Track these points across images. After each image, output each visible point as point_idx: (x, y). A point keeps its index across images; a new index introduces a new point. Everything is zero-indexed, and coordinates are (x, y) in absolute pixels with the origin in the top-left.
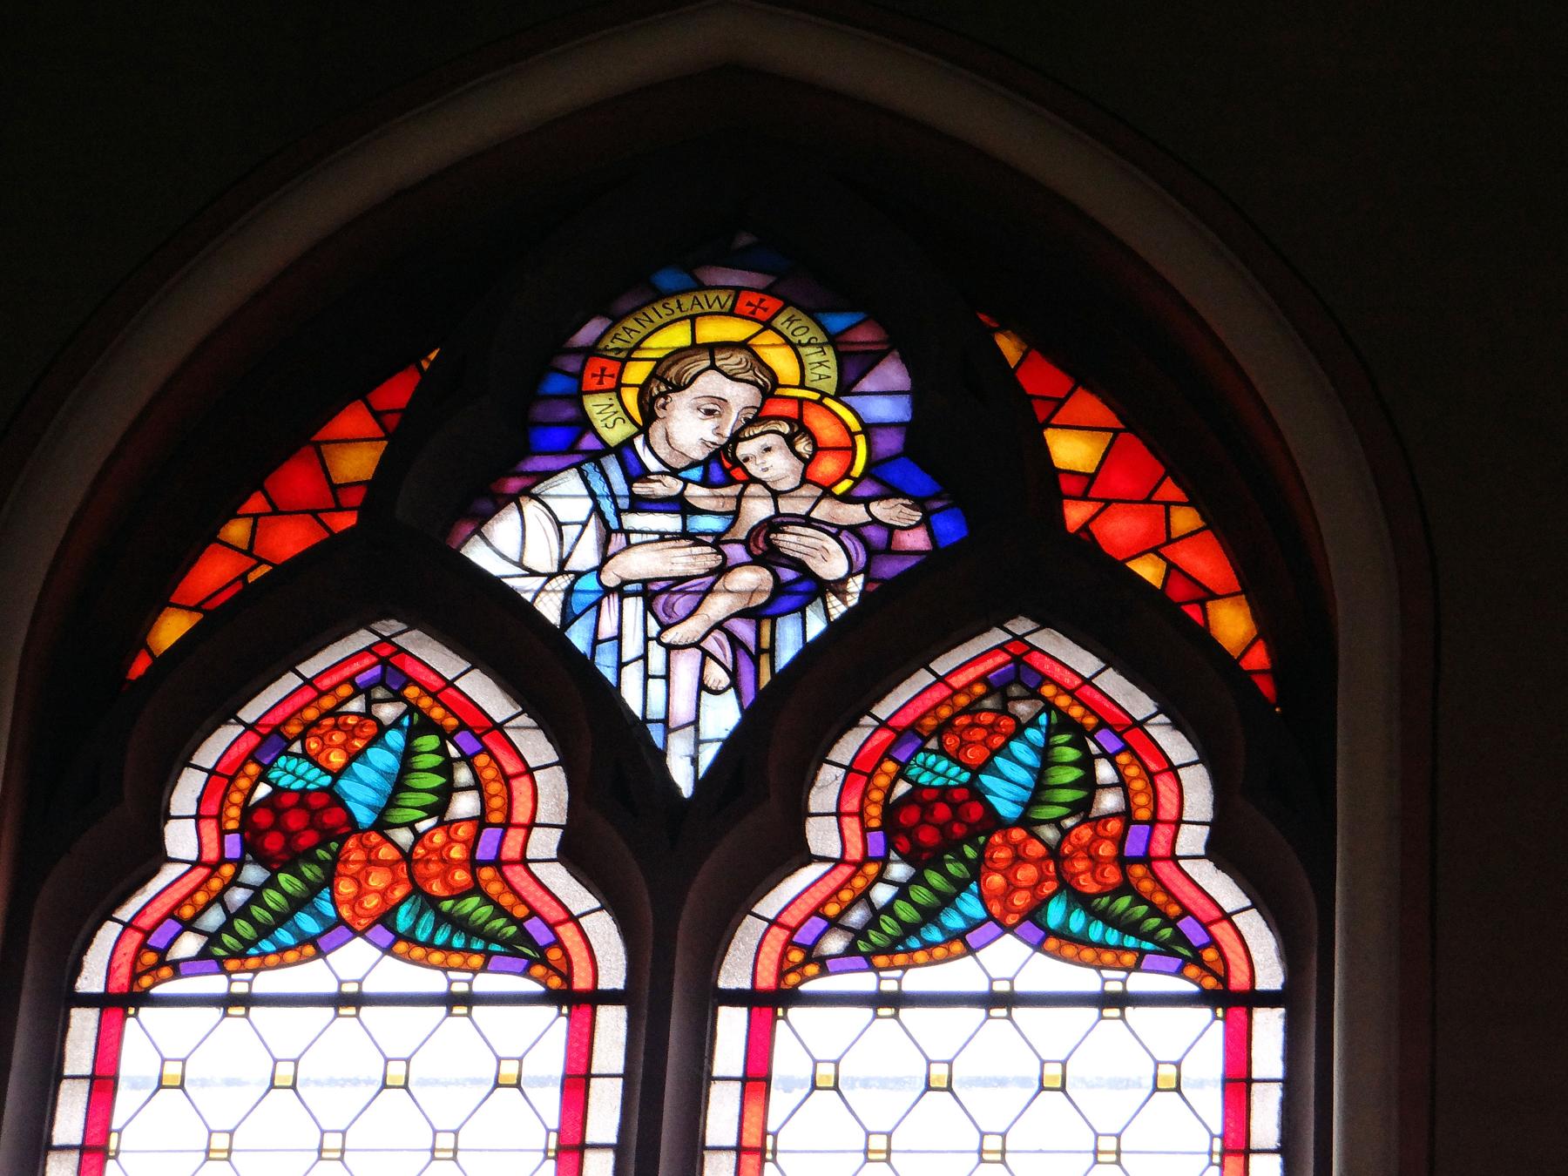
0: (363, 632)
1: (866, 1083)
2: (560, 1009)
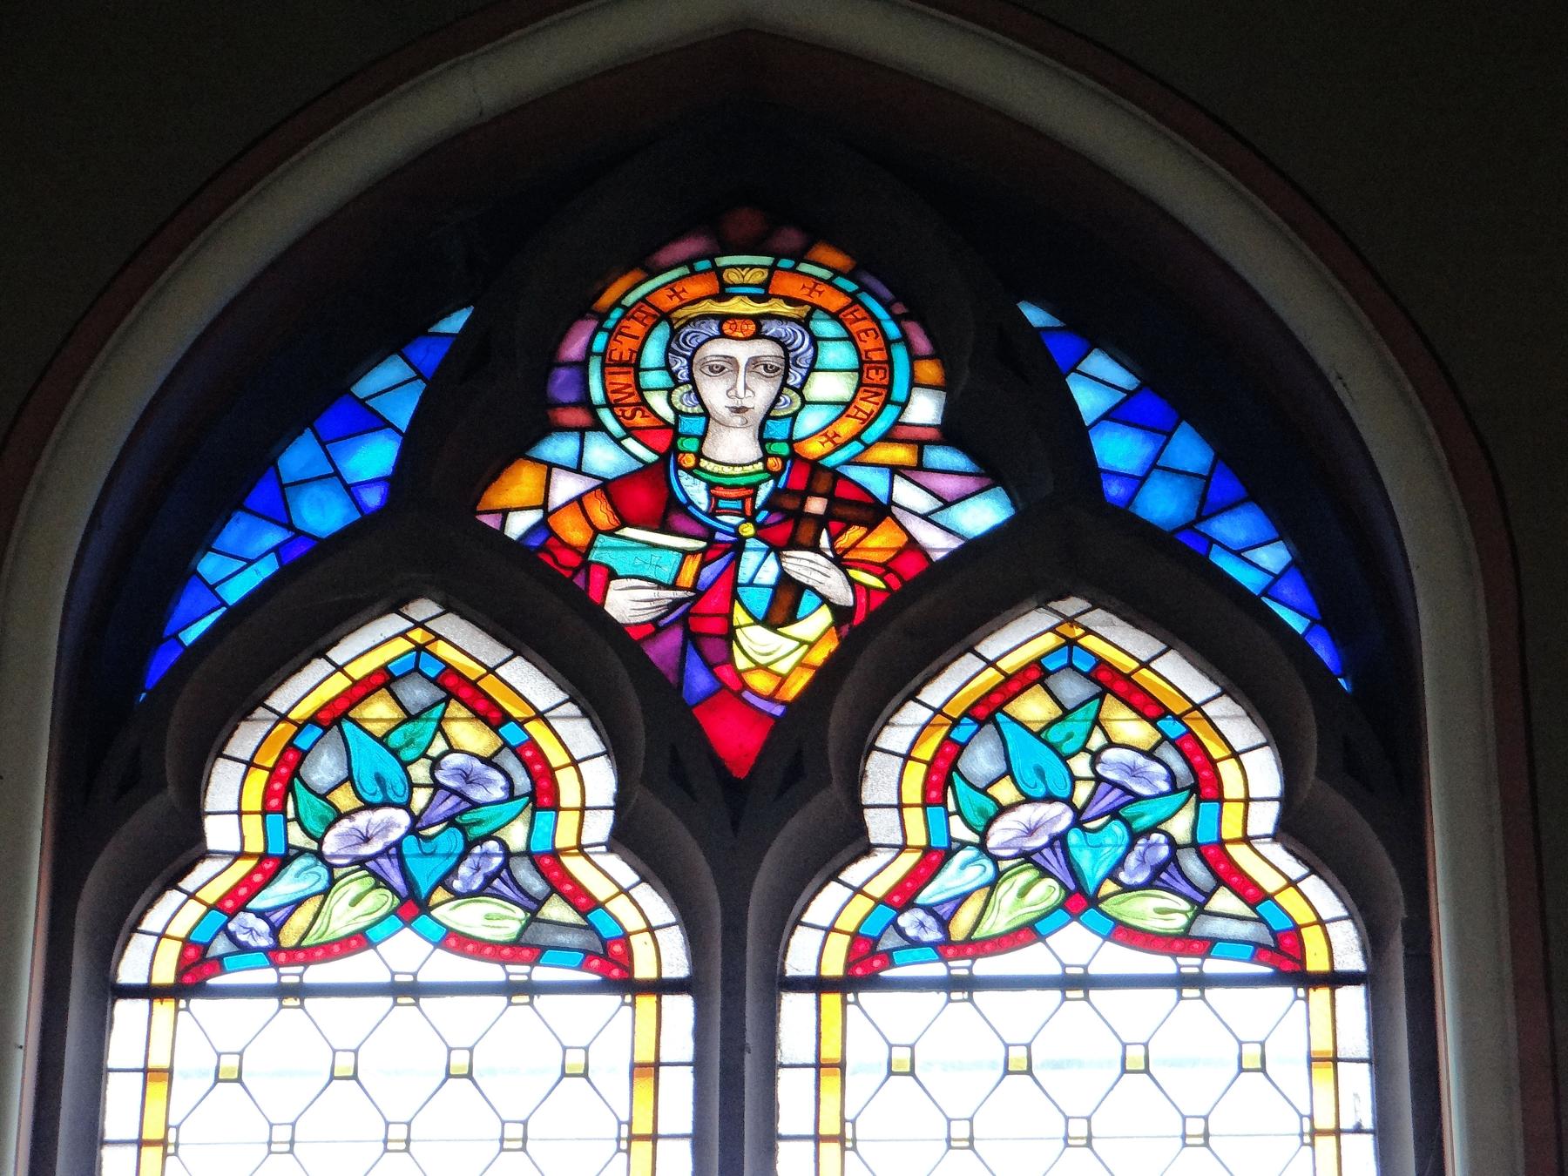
0: (394, 617)
1: (1057, 1065)
2: (177, 1003)
